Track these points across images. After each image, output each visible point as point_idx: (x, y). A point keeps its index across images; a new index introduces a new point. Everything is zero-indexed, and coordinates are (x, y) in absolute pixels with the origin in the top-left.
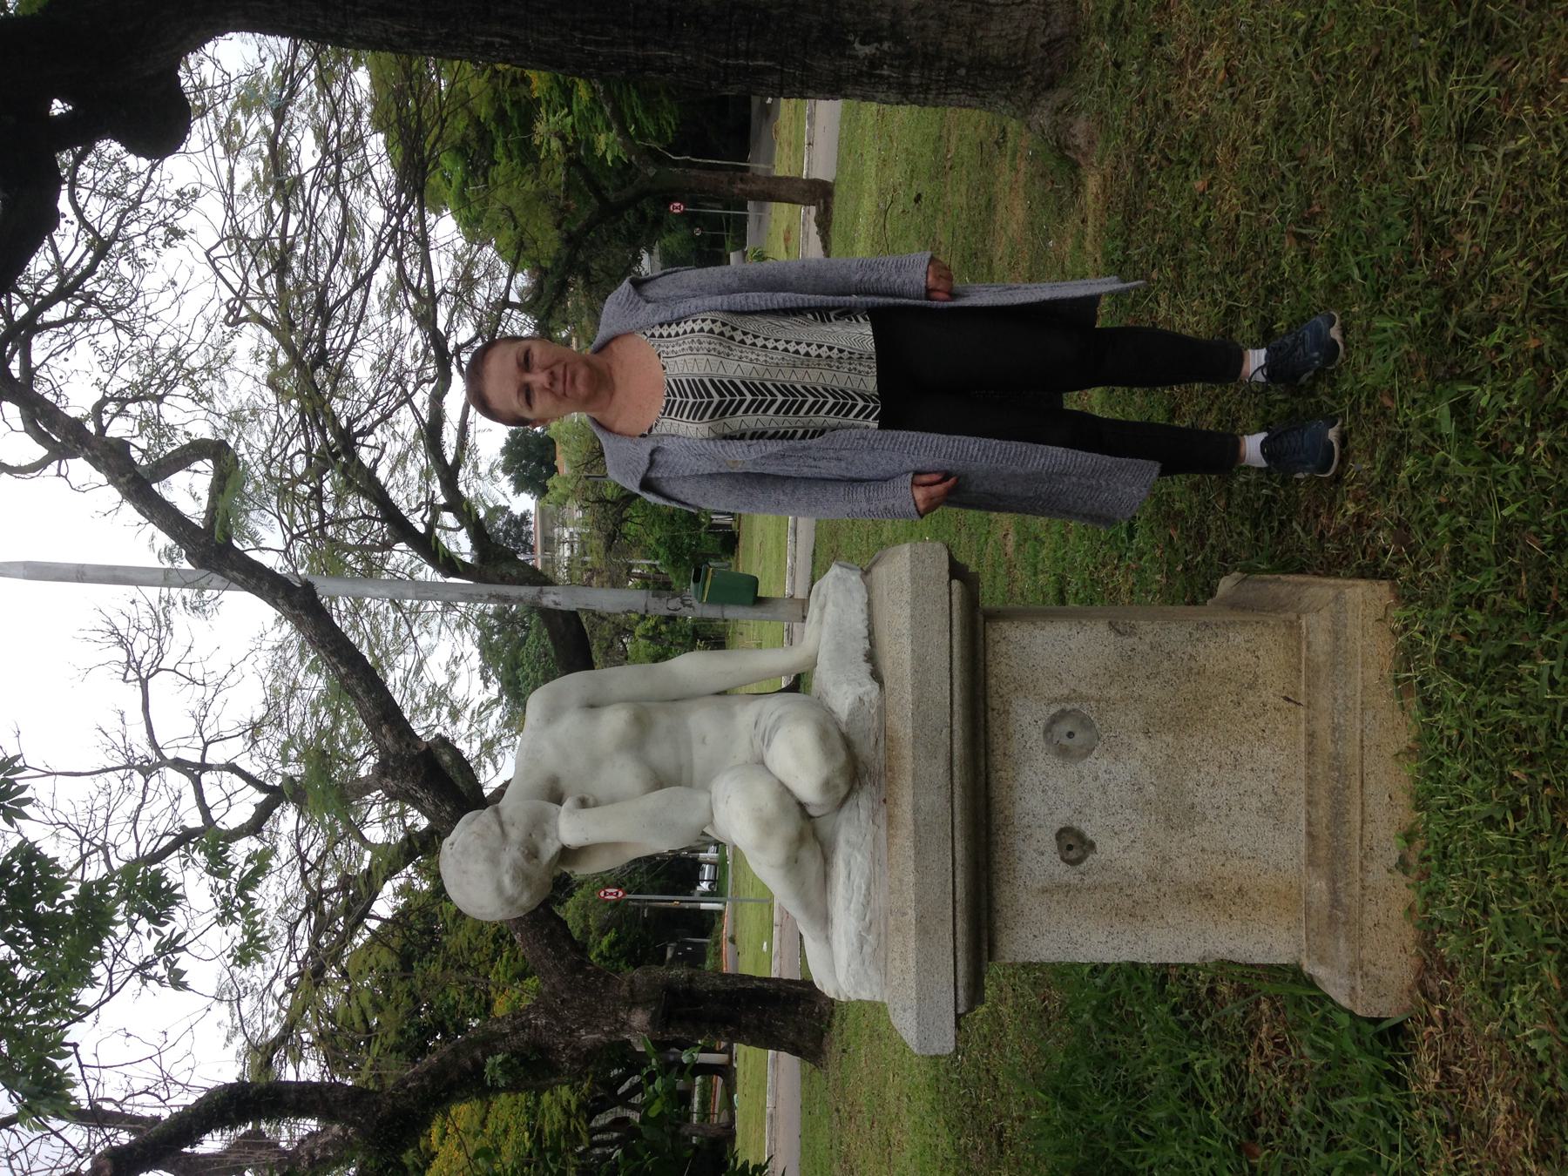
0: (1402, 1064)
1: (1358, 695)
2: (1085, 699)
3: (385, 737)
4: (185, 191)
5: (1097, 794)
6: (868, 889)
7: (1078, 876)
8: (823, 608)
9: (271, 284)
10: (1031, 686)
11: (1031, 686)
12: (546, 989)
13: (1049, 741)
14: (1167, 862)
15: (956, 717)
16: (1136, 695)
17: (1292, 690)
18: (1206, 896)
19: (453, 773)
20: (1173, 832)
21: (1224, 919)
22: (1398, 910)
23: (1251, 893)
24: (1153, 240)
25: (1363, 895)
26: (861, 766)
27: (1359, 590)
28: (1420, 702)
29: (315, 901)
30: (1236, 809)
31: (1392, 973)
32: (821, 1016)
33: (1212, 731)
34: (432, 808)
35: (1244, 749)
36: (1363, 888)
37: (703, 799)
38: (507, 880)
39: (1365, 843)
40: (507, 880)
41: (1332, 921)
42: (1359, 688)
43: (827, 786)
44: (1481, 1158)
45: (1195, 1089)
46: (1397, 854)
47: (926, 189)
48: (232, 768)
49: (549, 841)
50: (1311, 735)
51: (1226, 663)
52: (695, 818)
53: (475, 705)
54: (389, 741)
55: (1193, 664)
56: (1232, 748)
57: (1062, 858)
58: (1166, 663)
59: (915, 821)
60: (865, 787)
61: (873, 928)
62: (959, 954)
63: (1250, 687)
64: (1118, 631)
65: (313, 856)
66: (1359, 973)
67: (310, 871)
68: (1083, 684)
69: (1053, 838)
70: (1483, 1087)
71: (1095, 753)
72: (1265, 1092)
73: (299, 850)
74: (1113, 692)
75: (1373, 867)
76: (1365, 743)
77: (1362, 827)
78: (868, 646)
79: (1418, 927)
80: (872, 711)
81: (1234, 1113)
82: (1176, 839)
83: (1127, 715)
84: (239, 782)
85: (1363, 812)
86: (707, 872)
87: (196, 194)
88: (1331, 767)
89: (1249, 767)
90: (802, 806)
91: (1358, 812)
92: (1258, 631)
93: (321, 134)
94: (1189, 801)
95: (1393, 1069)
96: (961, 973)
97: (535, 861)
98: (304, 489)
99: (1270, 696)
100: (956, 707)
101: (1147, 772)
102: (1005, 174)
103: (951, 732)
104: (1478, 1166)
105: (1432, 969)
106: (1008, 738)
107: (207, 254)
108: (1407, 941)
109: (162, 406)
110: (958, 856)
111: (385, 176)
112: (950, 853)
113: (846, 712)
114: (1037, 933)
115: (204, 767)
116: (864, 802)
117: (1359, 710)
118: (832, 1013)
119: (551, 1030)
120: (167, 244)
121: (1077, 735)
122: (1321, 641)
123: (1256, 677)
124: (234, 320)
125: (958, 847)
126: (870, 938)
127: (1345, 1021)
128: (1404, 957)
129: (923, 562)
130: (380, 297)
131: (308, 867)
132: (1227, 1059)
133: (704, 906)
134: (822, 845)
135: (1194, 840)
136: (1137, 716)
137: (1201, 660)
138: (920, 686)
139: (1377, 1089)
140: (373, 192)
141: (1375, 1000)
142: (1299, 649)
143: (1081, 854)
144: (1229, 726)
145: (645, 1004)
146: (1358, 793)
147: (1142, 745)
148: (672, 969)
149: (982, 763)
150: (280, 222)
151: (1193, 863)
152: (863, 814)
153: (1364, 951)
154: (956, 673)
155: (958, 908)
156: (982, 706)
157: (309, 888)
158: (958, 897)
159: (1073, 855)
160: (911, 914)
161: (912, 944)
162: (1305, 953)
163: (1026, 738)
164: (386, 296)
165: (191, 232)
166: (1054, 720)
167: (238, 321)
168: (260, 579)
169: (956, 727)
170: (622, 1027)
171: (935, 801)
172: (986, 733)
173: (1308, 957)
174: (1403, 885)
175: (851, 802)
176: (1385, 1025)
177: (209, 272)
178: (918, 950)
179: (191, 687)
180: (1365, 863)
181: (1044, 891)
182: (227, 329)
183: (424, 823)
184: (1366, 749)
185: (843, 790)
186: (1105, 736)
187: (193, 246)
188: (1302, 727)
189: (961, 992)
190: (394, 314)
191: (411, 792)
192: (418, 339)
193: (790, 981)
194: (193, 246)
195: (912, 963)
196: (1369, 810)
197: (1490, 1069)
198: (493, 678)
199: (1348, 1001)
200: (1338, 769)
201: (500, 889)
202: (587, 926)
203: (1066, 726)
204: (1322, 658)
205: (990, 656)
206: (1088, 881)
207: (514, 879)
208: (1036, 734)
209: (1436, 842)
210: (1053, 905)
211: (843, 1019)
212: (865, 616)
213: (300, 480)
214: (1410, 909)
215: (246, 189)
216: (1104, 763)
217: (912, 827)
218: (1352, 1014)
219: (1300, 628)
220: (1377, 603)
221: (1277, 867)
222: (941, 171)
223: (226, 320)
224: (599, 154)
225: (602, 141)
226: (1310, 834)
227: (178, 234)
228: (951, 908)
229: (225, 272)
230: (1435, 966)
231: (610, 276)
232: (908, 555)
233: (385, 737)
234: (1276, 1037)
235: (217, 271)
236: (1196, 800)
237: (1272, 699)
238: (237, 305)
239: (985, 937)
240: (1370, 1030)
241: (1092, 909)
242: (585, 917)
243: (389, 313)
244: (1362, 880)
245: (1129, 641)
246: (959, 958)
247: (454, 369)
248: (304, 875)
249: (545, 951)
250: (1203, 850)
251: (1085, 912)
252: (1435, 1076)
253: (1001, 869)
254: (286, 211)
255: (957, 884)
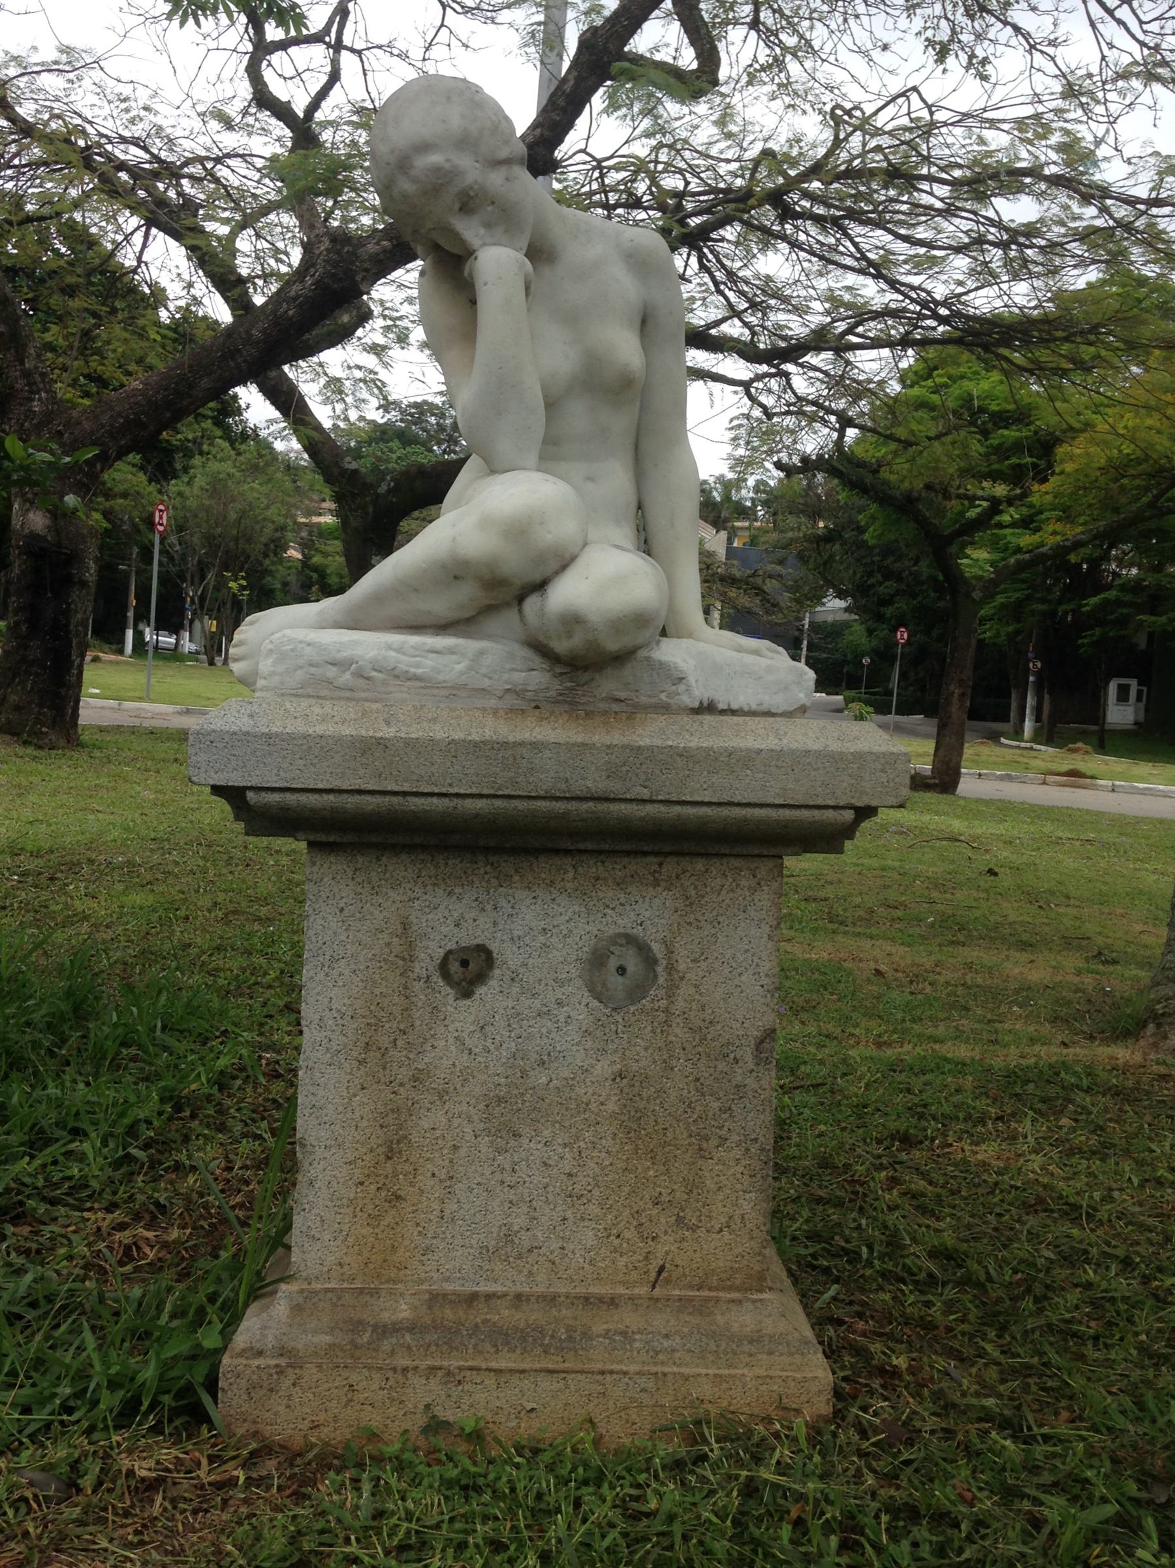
0: (151, 1421)
1: (675, 1369)
2: (671, 991)
3: (377, 243)
4: (988, 67)
5: (537, 1004)
6: (416, 678)
7: (424, 973)
8: (757, 652)
9: (877, 161)
10: (691, 918)
11: (691, 918)
12: (75, 414)
13: (614, 940)
14: (441, 1097)
15: (663, 808)
16: (674, 1063)
17: (674, 1275)
18: (391, 1149)
19: (328, 325)
20: (481, 1106)
21: (358, 1174)
22: (374, 1419)
23: (393, 1212)
24: (1110, 1120)
25: (394, 1370)
26: (586, 676)
27: (820, 1373)
28: (679, 1456)
29: (172, 172)
30: (511, 1195)
31: (281, 1409)
32: (39, 734)
33: (622, 1165)
34: (293, 293)
35: (594, 1209)
36: (405, 1370)
37: (533, 458)
38: (435, 159)
39: (468, 1373)
40: (436, 158)
41: (357, 1326)
42: (685, 1370)
43: (573, 621)
44: (40, 1537)
45: (48, 1142)
46: (451, 1419)
47: (1006, 880)
48: (334, 77)
49: (482, 231)
50: (612, 1302)
51: (713, 1187)
52: (504, 446)
53: (383, 375)
54: (371, 248)
55: (714, 1142)
56: (596, 1192)
57: (450, 952)
58: (716, 1105)
59: (522, 744)
60: (557, 681)
61: (362, 681)
62: (331, 797)
63: (680, 1220)
64: (762, 1042)
65: (222, 172)
66: (283, 1362)
67: (205, 168)
68: (692, 990)
69: (479, 941)
70: (142, 1543)
71: (596, 1003)
72: (63, 1231)
73: (229, 156)
74: (679, 1031)
75: (434, 1384)
76: (608, 1378)
77: (489, 1370)
78: (721, 706)
79: (347, 1446)
80: (663, 696)
81: (28, 1191)
82: (473, 1111)
83: (646, 1049)
84: (315, 88)
85: (511, 1371)
86: (167, 640)
87: (984, 78)
88: (570, 1329)
89: (569, 1214)
90: (541, 586)
91: (511, 1365)
92: (756, 1233)
93: (1031, 230)
94: (526, 1131)
95: (143, 1408)
96: (304, 798)
97: (457, 206)
98: (641, 187)
99: (666, 1247)
100: (677, 809)
101: (566, 1073)
102: (1072, 961)
103: (644, 801)
104: (26, 1534)
105: (292, 1465)
106: (620, 884)
107: (915, 89)
108: (326, 1430)
109: (745, 29)
110: (469, 803)
111: (977, 303)
112: (474, 791)
113: (664, 658)
114: (346, 912)
115: (338, 46)
116: (538, 678)
117: (654, 1369)
118: (40, 747)
119: (27, 417)
120: (930, 43)
121: (620, 979)
122: (743, 1319)
123: (694, 1229)
124: (837, 118)
125: (481, 804)
126: (347, 676)
127: (209, 1339)
128: (306, 1425)
129: (883, 771)
130: (849, 289)
131: (209, 165)
132: (95, 1184)
133: (130, 633)
134: (469, 621)
135: (469, 1136)
136: (643, 1063)
137: (721, 1153)
138: (711, 759)
139: (113, 1385)
140: (960, 290)
141: (243, 1383)
142: (730, 1289)
143: (456, 978)
144: (627, 1189)
145: (55, 528)
146: (538, 1366)
147: (603, 1068)
148: (95, 562)
149: (589, 846)
150: (944, 176)
151: (438, 1133)
152: (519, 677)
153: (315, 1371)
154: (725, 812)
155: (395, 800)
156: (667, 849)
157: (186, 163)
158: (410, 799)
159: (454, 967)
160: (389, 732)
161: (347, 731)
162: (305, 1286)
163: (619, 909)
164: (847, 297)
165: (945, 71)
166: (643, 949)
167: (838, 122)
168: (564, 110)
169: (650, 809)
170: (28, 500)
171: (547, 778)
172: (628, 853)
173: (302, 1291)
174: (407, 1425)
175: (537, 660)
176: (206, 1399)
177: (895, 89)
178: (339, 740)
179: (422, 44)
180: (440, 1373)
181: (406, 926)
182: (828, 108)
183: (259, 300)
184: (600, 1377)
185: (561, 646)
186: (619, 1018)
187: (925, 73)
188: (621, 1290)
189: (276, 797)
190: (827, 305)
191: (312, 270)
192: (797, 327)
193: (77, 701)
194: (925, 73)
195: (320, 729)
196: (515, 1379)
197: (172, 1553)
198: (388, 416)
199: (242, 1346)
200: (570, 1338)
201: (424, 147)
202: (115, 496)
203: (633, 964)
204: (720, 1319)
205: (735, 862)
206: (418, 986)
207: (437, 170)
208: (624, 922)
209: (485, 1476)
210: (385, 937)
211: (34, 758)
212: (754, 707)
213: (654, 182)
214: (374, 1437)
215: (982, 141)
216: (581, 1015)
217: (511, 739)
218: (218, 1352)
219: (760, 1291)
220: (804, 1398)
221: (427, 1250)
222: (1032, 897)
223: (838, 106)
224: (968, 551)
225: (982, 554)
226: (474, 1296)
227: (942, 53)
228: (396, 788)
229: (891, 110)
230: (296, 1470)
231: (825, 564)
232: (894, 750)
233: (377, 243)
234: (139, 1249)
235: (894, 99)
236: (525, 1141)
237: (661, 1250)
238: (853, 121)
239: (348, 838)
240: (199, 1374)
241: (377, 991)
242: (125, 495)
243: (827, 300)
244: (416, 1368)
245: (747, 1054)
246: (325, 797)
247: (764, 368)
248: (201, 160)
249: (119, 415)
250: (455, 1147)
251: (375, 982)
252: (144, 1469)
253: (437, 867)
254: (954, 183)
255: (430, 800)
